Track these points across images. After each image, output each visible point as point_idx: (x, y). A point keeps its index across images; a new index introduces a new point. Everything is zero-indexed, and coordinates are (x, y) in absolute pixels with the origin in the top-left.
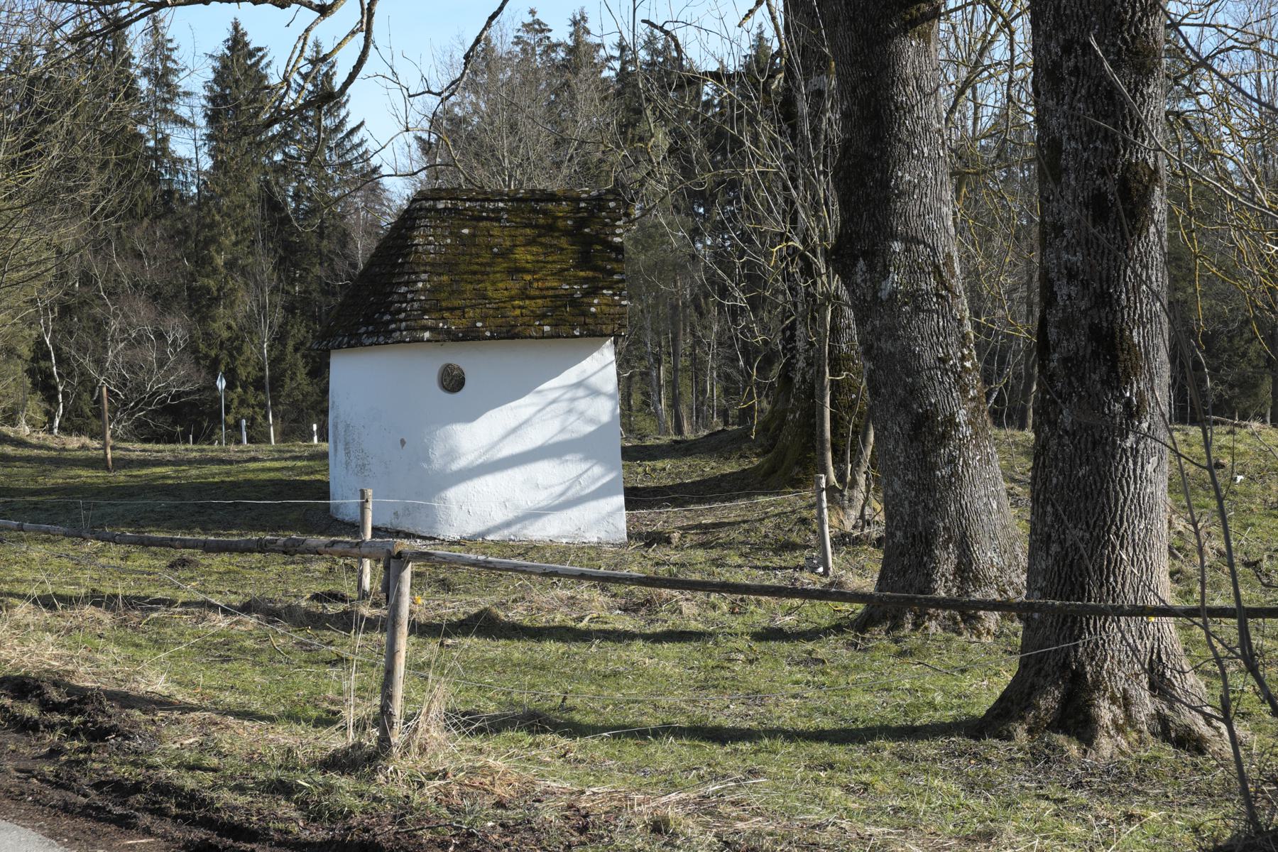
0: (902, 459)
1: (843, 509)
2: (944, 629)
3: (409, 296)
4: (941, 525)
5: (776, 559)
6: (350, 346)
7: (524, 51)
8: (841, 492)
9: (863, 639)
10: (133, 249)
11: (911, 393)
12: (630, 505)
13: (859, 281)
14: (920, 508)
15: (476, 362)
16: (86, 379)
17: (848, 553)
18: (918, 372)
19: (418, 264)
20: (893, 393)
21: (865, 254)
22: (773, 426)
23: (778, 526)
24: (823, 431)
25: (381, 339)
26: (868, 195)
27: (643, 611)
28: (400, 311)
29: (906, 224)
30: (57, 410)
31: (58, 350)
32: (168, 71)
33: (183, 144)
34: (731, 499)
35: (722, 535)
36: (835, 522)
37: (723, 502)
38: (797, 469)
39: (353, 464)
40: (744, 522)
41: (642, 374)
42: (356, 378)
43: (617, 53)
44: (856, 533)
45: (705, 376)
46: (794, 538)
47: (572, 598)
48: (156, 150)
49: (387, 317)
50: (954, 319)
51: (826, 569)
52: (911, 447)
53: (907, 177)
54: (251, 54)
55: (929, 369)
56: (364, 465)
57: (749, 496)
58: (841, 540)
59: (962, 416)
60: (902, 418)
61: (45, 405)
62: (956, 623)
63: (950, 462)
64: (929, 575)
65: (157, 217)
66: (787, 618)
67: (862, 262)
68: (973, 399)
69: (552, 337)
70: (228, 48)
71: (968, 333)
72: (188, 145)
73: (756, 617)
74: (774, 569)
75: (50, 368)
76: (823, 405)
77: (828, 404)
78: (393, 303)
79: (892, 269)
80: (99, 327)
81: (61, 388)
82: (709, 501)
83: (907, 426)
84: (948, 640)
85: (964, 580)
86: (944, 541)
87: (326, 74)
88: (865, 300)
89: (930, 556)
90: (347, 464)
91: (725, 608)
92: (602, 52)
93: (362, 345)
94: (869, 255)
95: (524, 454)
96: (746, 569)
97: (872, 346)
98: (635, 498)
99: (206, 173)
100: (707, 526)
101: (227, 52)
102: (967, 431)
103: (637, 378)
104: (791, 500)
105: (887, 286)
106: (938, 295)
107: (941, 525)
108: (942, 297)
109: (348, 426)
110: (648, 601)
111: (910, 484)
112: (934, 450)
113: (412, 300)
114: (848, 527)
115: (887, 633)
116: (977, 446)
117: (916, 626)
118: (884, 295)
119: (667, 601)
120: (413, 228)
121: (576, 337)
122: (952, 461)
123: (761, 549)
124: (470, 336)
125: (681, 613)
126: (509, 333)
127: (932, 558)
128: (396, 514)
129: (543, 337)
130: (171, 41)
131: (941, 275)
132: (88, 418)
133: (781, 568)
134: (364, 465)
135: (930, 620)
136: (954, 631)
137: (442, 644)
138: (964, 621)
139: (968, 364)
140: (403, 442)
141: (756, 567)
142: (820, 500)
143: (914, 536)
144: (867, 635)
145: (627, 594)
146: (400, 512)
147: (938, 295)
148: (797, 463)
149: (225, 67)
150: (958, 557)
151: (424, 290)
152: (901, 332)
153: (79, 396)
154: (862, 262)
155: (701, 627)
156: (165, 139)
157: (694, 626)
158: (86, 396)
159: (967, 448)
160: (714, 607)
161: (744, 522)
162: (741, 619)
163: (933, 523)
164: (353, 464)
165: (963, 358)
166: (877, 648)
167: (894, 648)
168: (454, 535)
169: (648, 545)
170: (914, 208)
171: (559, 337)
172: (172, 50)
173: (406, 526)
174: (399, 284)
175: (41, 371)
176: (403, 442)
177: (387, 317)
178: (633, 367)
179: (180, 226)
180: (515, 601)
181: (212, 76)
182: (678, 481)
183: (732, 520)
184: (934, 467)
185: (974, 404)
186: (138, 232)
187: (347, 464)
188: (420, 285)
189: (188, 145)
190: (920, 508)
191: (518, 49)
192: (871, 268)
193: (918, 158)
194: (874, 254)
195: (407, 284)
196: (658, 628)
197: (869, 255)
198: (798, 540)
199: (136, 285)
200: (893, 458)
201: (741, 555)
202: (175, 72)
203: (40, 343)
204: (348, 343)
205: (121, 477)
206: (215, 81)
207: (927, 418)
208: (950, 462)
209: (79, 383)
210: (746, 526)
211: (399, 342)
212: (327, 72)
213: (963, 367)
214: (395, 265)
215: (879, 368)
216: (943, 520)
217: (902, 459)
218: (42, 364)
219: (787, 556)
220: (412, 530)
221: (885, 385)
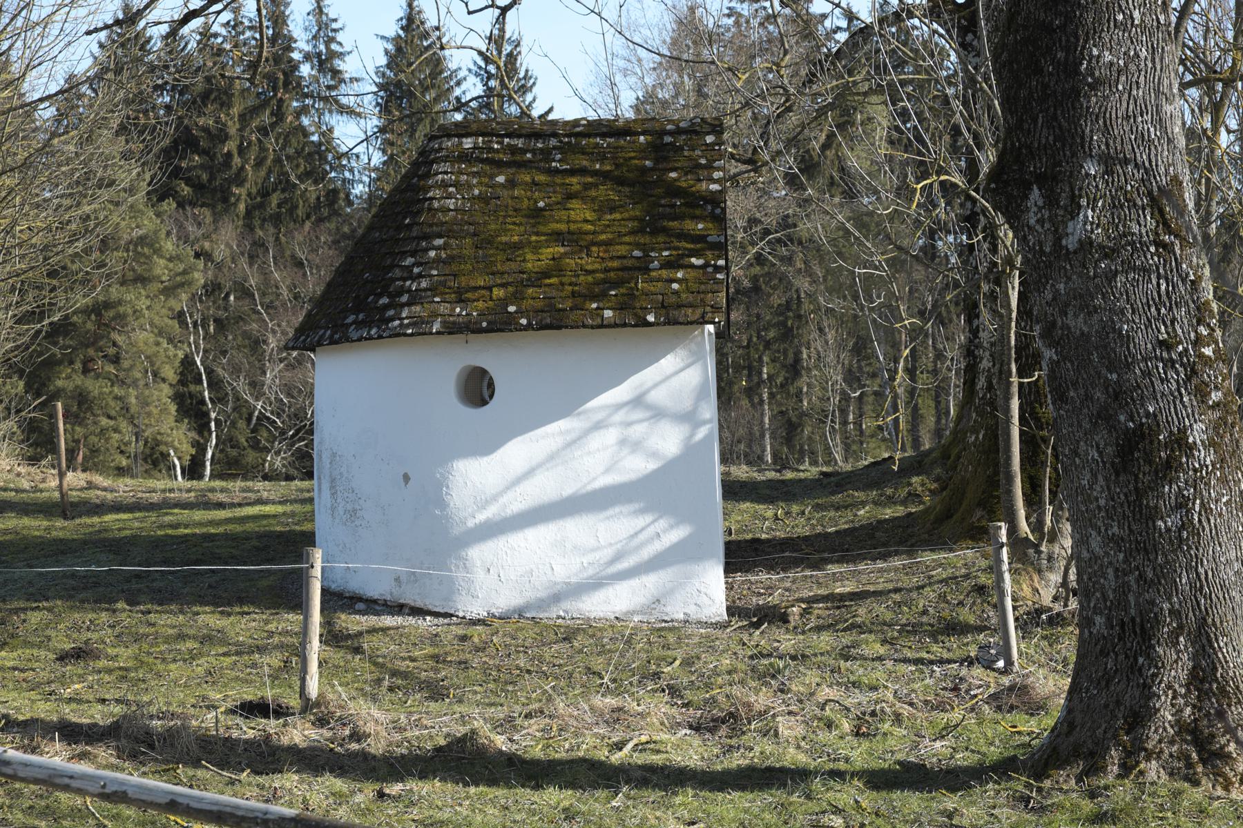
0: (1102, 502)
1: (1040, 571)
2: (1171, 774)
3: (416, 270)
4: (1166, 606)
5: (935, 648)
6: (333, 342)
7: (737, 23)
8: (1036, 547)
9: (1040, 790)
10: (293, 256)
11: (1116, 396)
12: (729, 569)
13: (1032, 222)
14: (1131, 579)
15: (512, 362)
16: (241, 407)
17: (1044, 638)
18: (1128, 365)
19: (431, 226)
20: (1088, 397)
21: (1041, 179)
22: (955, 452)
23: (942, 597)
24: (1009, 458)
25: (373, 332)
26: (1045, 86)
27: (723, 730)
28: (400, 292)
29: (1106, 130)
30: (208, 440)
31: (210, 372)
32: (333, 55)
33: (349, 133)
34: (884, 557)
35: (862, 613)
36: (1026, 591)
37: (874, 559)
38: (979, 513)
39: (341, 510)
40: (897, 590)
41: (876, 393)
42: (356, 392)
43: (844, 24)
44: (1057, 608)
45: (948, 394)
46: (967, 616)
47: (620, 709)
48: (320, 144)
49: (384, 301)
50: (1184, 281)
51: (1009, 662)
52: (1117, 482)
53: (1108, 57)
54: (426, 35)
55: (1145, 360)
56: (355, 511)
57: (911, 554)
58: (1032, 620)
59: (1197, 433)
60: (1101, 437)
61: (193, 435)
62: (1190, 765)
63: (1179, 506)
64: (1146, 687)
65: (321, 220)
66: (938, 744)
67: (1036, 191)
68: (1217, 405)
69: (615, 325)
70: (402, 28)
71: (1207, 303)
72: (354, 135)
73: (891, 742)
74: (932, 662)
75: (202, 393)
76: (1008, 421)
77: (1016, 420)
78: (394, 280)
79: (1084, 202)
80: (255, 344)
81: (213, 415)
82: (853, 560)
83: (1109, 450)
84: (1177, 794)
85: (1204, 695)
86: (1171, 633)
87: (510, 55)
88: (1042, 252)
89: (1148, 656)
90: (333, 509)
91: (846, 726)
92: (827, 23)
93: (349, 340)
94: (1048, 181)
95: (571, 495)
96: (889, 664)
97: (1054, 324)
98: (741, 556)
99: (376, 169)
100: (842, 597)
101: (401, 32)
102: (1207, 457)
103: (871, 399)
104: (965, 556)
105: (1076, 231)
106: (1159, 244)
107: (1166, 606)
108: (1165, 246)
109: (334, 455)
110: (731, 715)
111: (1116, 541)
112: (1155, 486)
113: (420, 276)
114: (1046, 598)
115: (1079, 780)
116: (1224, 481)
117: (1126, 770)
118: (1071, 243)
119: (760, 714)
120: (428, 175)
121: (650, 324)
122: (1182, 504)
123: (915, 632)
124: (499, 324)
125: (776, 735)
126: (552, 320)
127: (1153, 660)
128: (397, 580)
129: (601, 326)
130: (335, 20)
131: (1162, 212)
132: (244, 449)
133: (941, 662)
134: (355, 511)
135: (1148, 759)
136: (1187, 779)
137: (381, 795)
138: (1204, 761)
139: (1208, 351)
140: (406, 478)
141: (906, 661)
142: (999, 561)
143: (1122, 624)
144: (1047, 784)
145: (706, 701)
146: (404, 578)
147: (1159, 244)
148: (979, 505)
149: (399, 49)
150: (1194, 657)
151: (438, 260)
152: (1099, 301)
153: (233, 424)
154: (1036, 191)
155: (802, 759)
156: (331, 130)
157: (794, 757)
158: (241, 424)
159: (1207, 484)
160: (830, 725)
161: (897, 590)
162: (865, 744)
163: (1152, 603)
164: (341, 510)
165: (1198, 342)
166: (1060, 806)
167: (1087, 806)
168: (476, 610)
169: (757, 625)
170: (1118, 106)
171: (625, 325)
172: (335, 31)
173: (411, 596)
174: (404, 254)
175: (191, 395)
176: (406, 478)
177: (384, 301)
178: (864, 386)
179: (346, 229)
180: (528, 716)
181: (383, 61)
182: (819, 529)
183: (880, 587)
184: (1154, 514)
185: (1218, 414)
186: (299, 237)
187: (333, 509)
188: (432, 254)
189: (354, 135)
190: (1131, 579)
191: (731, 21)
192: (1051, 201)
193: (1123, 27)
194: (1055, 178)
195: (413, 254)
196: (737, 761)
197: (1048, 181)
198: (972, 620)
199: (296, 297)
200: (1089, 500)
201: (884, 642)
202: (341, 55)
203: (188, 362)
204: (331, 337)
205: (61, 528)
206: (388, 66)
207: (1143, 436)
208: (1179, 506)
209: (234, 409)
210: (897, 597)
211: (398, 335)
212: (511, 52)
213: (1201, 356)
214: (400, 227)
215: (1065, 359)
216: (1169, 599)
217: (1102, 502)
218: (192, 388)
219: (953, 642)
220: (419, 604)
221: (1075, 384)
